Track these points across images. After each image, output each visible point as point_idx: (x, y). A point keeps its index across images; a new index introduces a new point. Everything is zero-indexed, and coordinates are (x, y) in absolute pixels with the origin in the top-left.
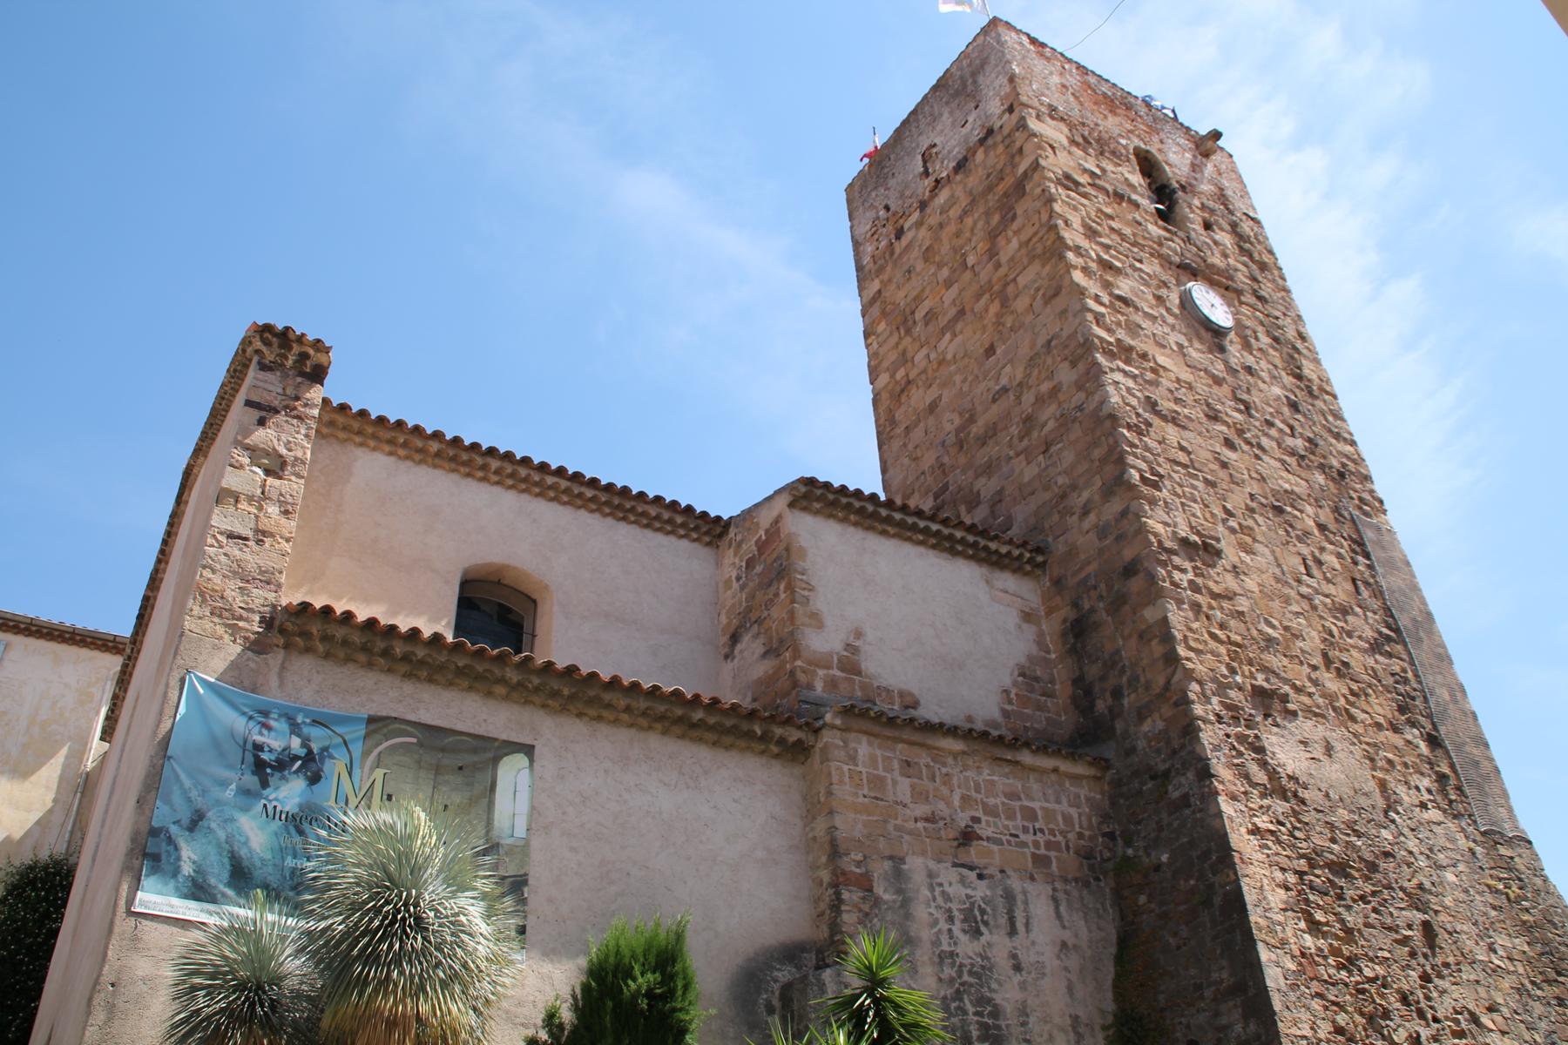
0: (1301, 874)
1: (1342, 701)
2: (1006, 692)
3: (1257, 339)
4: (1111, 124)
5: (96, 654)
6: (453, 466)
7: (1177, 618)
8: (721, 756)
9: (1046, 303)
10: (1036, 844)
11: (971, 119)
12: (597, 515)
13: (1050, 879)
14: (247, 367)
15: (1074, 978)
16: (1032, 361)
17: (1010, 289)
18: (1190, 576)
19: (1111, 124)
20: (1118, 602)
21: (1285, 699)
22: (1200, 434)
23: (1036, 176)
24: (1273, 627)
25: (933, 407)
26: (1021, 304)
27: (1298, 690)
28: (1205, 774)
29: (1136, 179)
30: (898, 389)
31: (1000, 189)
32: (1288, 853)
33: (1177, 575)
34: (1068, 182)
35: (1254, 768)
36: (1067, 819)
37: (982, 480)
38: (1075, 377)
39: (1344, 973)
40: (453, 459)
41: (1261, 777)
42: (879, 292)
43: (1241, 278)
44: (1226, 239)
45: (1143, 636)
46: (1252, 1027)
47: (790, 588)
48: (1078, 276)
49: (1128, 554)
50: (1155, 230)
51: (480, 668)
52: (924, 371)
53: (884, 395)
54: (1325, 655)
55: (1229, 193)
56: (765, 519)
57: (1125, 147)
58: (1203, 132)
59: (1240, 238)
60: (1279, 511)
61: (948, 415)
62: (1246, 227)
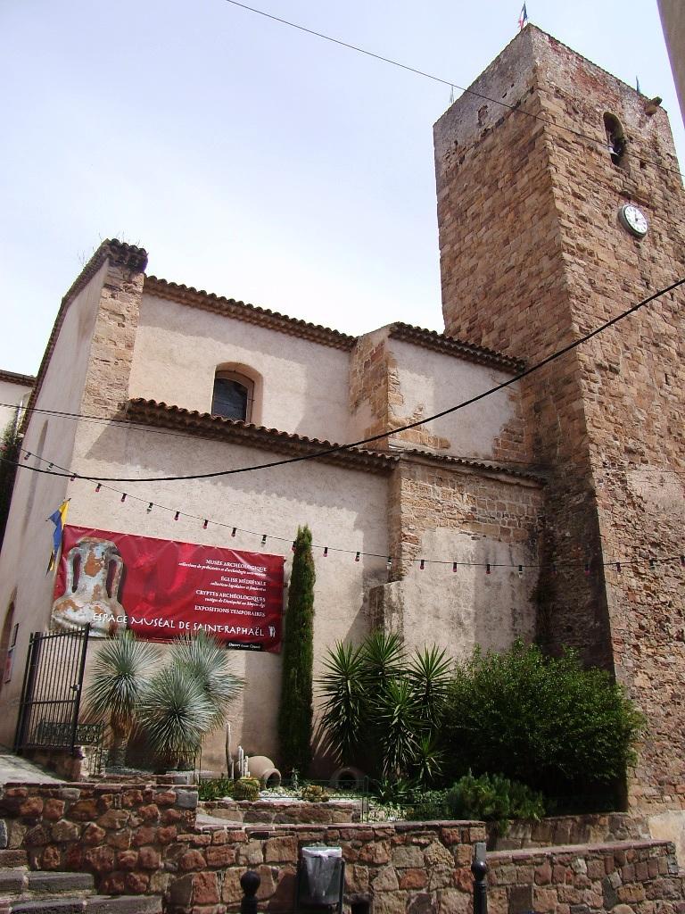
0: (635, 548)
1: (674, 455)
2: (497, 440)
3: (661, 238)
4: (592, 98)
5: (15, 386)
6: (211, 309)
7: (590, 407)
8: (346, 473)
9: (540, 219)
10: (504, 523)
11: (508, 93)
12: (287, 335)
13: (508, 541)
14: (103, 262)
15: (515, 590)
16: (528, 254)
17: (520, 207)
18: (600, 385)
19: (592, 98)
20: (559, 397)
21: (642, 454)
22: (617, 301)
23: (542, 137)
24: (642, 414)
25: (472, 271)
26: (526, 217)
27: (652, 449)
28: (592, 494)
29: (602, 134)
30: (454, 255)
31: (521, 143)
32: (631, 537)
33: (592, 385)
34: (562, 142)
35: (619, 491)
36: (521, 509)
37: (496, 317)
38: (550, 266)
39: (649, 598)
40: (211, 305)
41: (622, 496)
42: (448, 195)
43: (658, 198)
44: (651, 172)
45: (571, 418)
46: (598, 624)
47: (386, 382)
48: (559, 205)
49: (568, 371)
50: (609, 170)
51: (228, 430)
52: (470, 247)
53: (447, 259)
54: (669, 430)
55: (660, 140)
56: (376, 341)
57: (599, 114)
58: (651, 97)
59: (664, 172)
60: (656, 345)
61: (480, 277)
62: (666, 164)
